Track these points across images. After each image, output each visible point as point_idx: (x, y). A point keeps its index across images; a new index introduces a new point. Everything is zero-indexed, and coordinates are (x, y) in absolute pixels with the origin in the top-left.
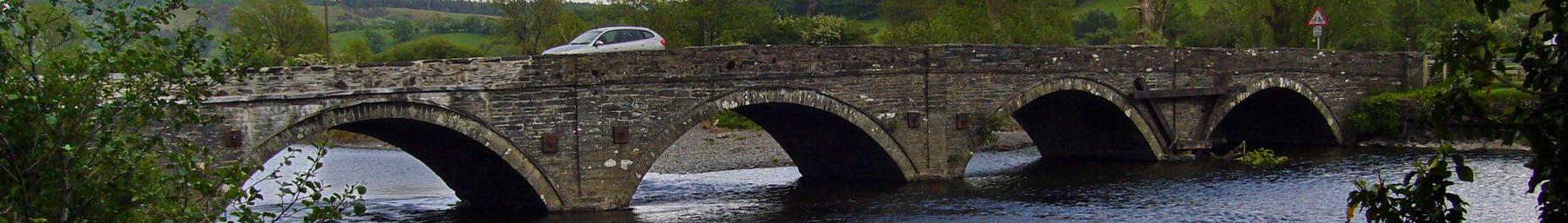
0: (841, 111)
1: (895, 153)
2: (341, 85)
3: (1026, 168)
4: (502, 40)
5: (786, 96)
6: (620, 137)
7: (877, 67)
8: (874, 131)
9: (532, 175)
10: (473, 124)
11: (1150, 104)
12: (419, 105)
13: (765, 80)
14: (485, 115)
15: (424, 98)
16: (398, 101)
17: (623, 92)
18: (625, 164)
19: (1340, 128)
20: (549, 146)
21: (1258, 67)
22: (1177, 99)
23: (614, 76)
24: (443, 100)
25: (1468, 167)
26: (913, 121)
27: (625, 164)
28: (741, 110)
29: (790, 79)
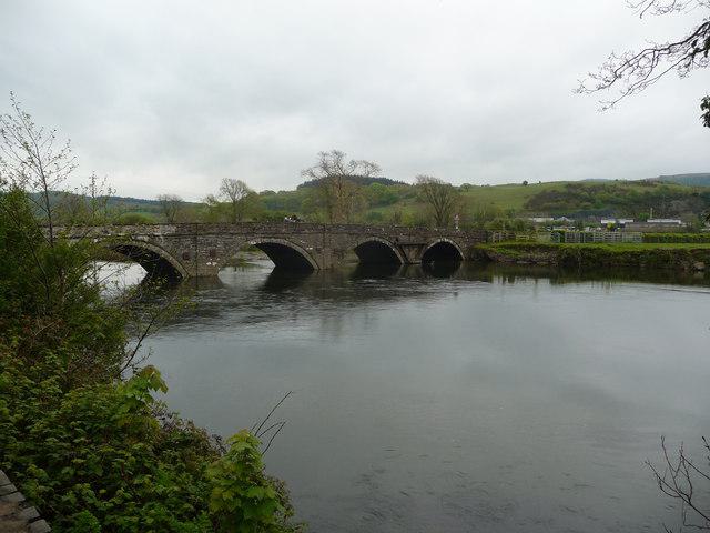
0: (294, 246)
1: (311, 261)
2: (107, 232)
3: (544, 191)
4: (102, 210)
5: (274, 240)
6: (213, 254)
7: (306, 231)
8: (305, 254)
9: (179, 267)
10: (157, 248)
11: (401, 247)
12: (138, 241)
13: (265, 234)
14: (162, 245)
15: (139, 238)
16: (127, 237)
17: (559, 224)
18: (214, 264)
19: (460, 190)
20: (186, 257)
21: (438, 234)
22: (411, 246)
23: (211, 231)
24: (146, 239)
25: (458, 267)
26: (318, 251)
27: (214, 264)
28: (257, 245)
29: (275, 235)
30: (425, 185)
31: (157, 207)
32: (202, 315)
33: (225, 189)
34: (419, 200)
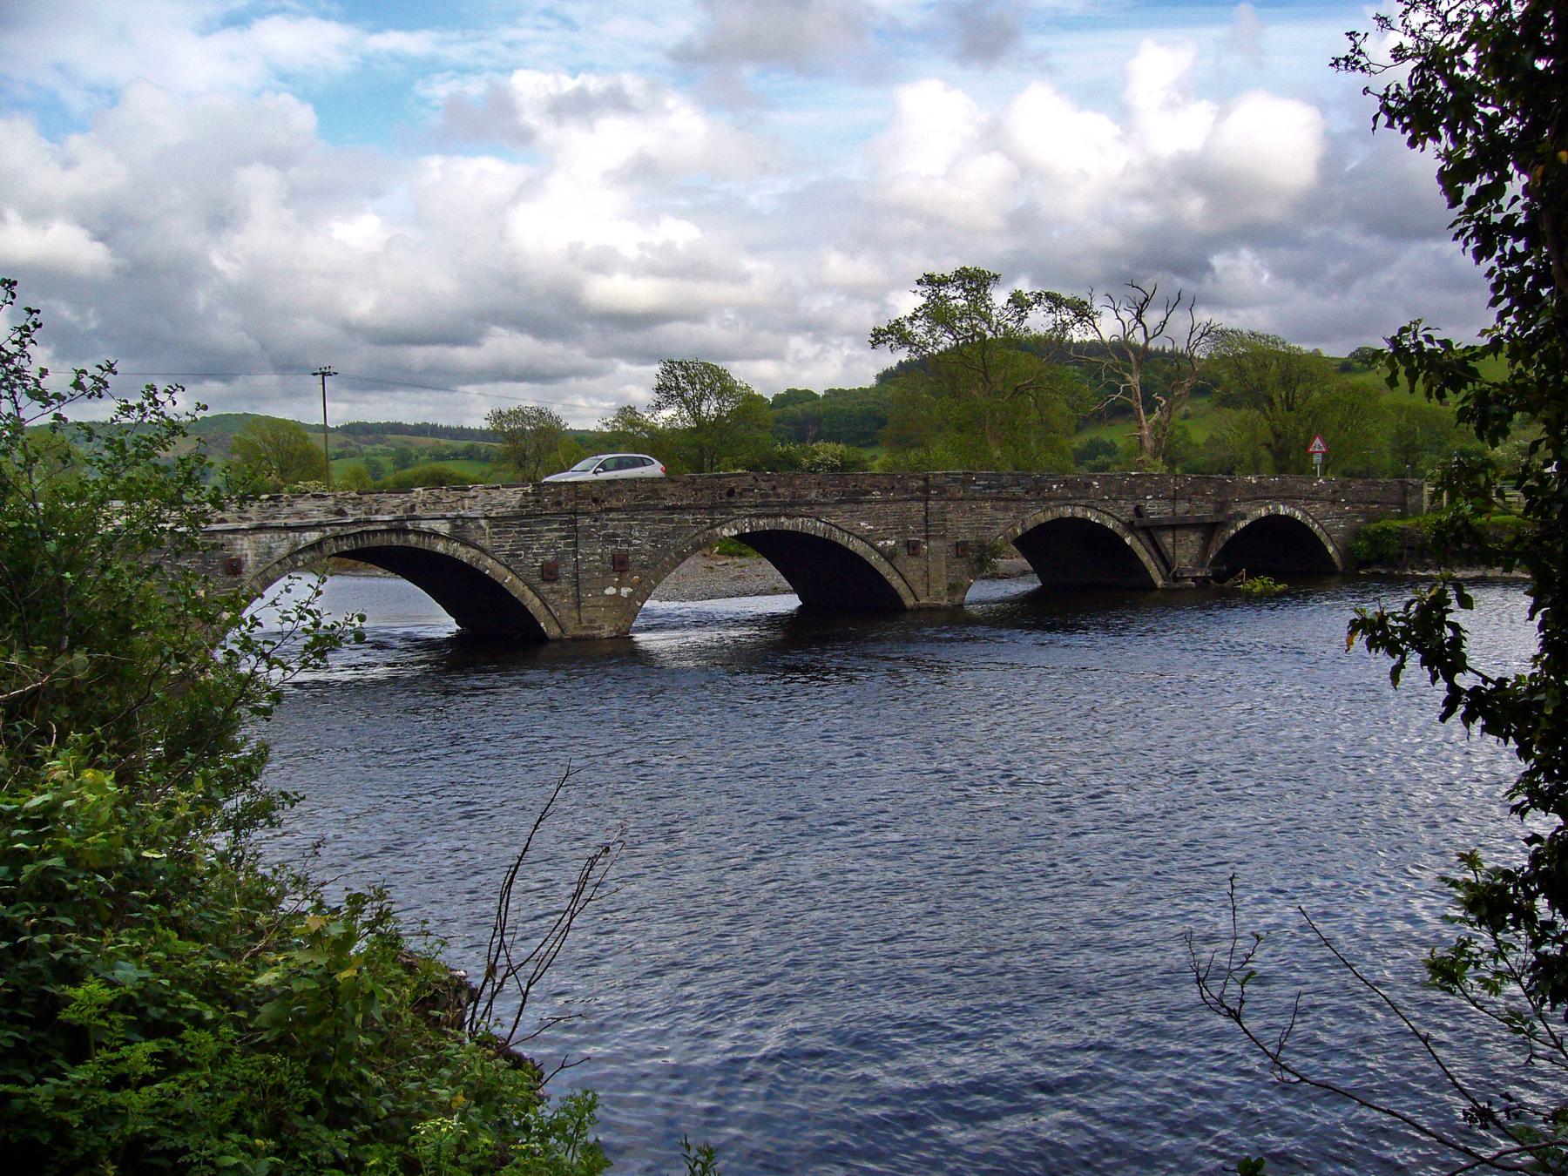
0: (842, 539)
1: (895, 581)
2: (341, 513)
5: (786, 523)
7: (877, 495)
8: (873, 558)
9: (532, 603)
10: (474, 552)
11: (1150, 531)
13: (764, 507)
14: (485, 543)
15: (424, 525)
16: (398, 528)
18: (625, 591)
20: (549, 574)
21: (1258, 495)
22: (1175, 527)
23: (614, 503)
24: (443, 528)
26: (913, 549)
27: (625, 591)
28: (741, 538)
29: (791, 506)
30: (511, 437)
31: (483, 445)
32: (1001, 578)
33: (667, 391)
34: (1227, 401)
